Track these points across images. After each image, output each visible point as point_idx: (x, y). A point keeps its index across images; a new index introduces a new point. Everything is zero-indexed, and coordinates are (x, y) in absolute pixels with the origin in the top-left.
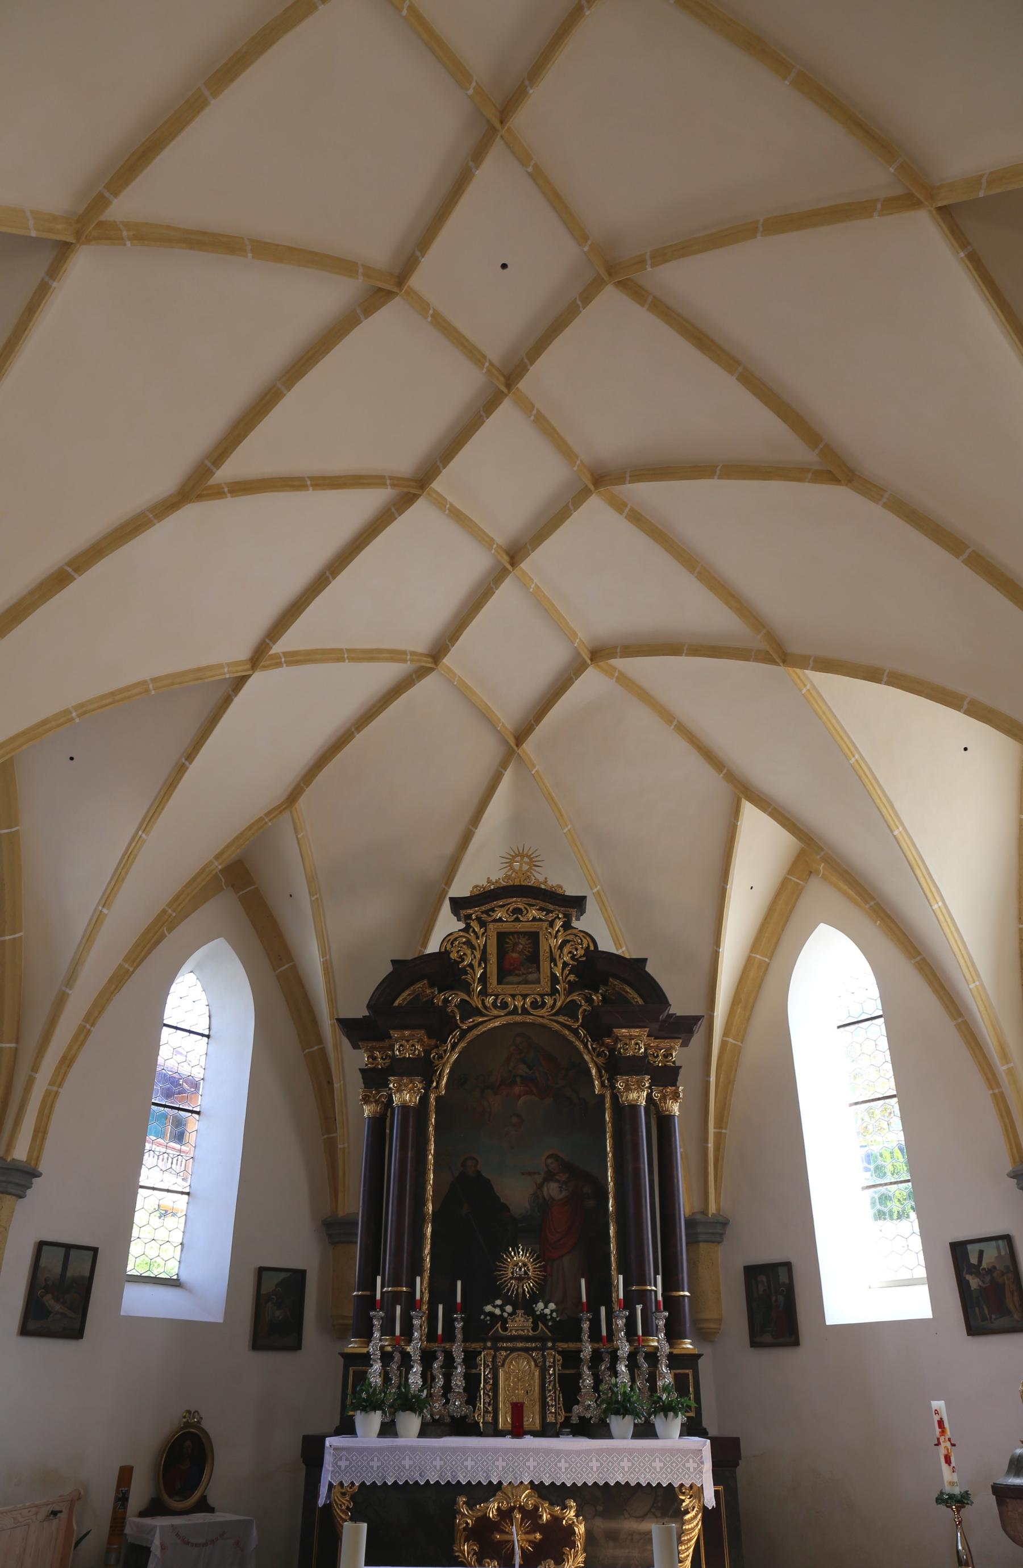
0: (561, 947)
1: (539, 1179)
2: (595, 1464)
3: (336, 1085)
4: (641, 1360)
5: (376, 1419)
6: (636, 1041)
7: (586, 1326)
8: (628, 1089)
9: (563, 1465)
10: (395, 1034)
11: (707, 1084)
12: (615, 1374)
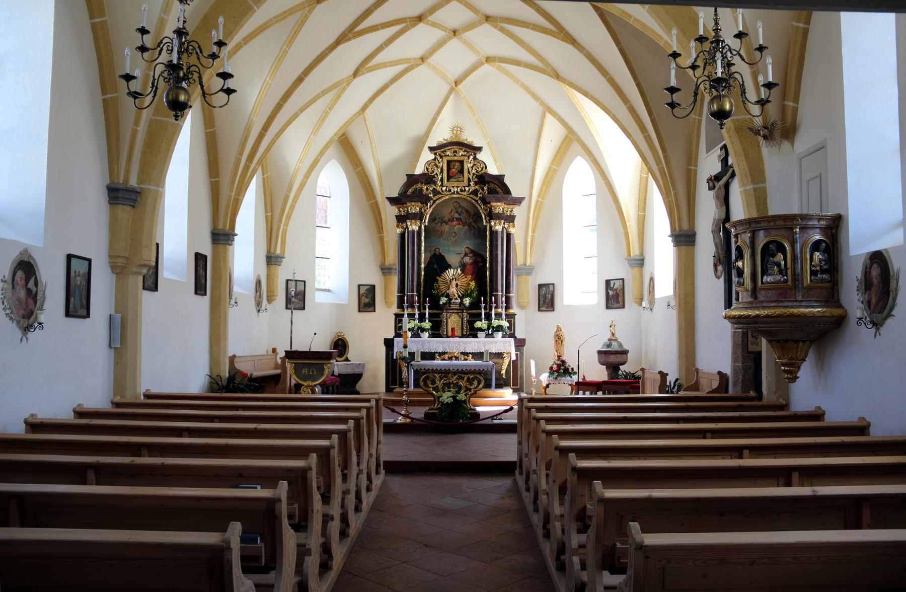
3: (383, 217)
6: (499, 207)
10: (408, 204)
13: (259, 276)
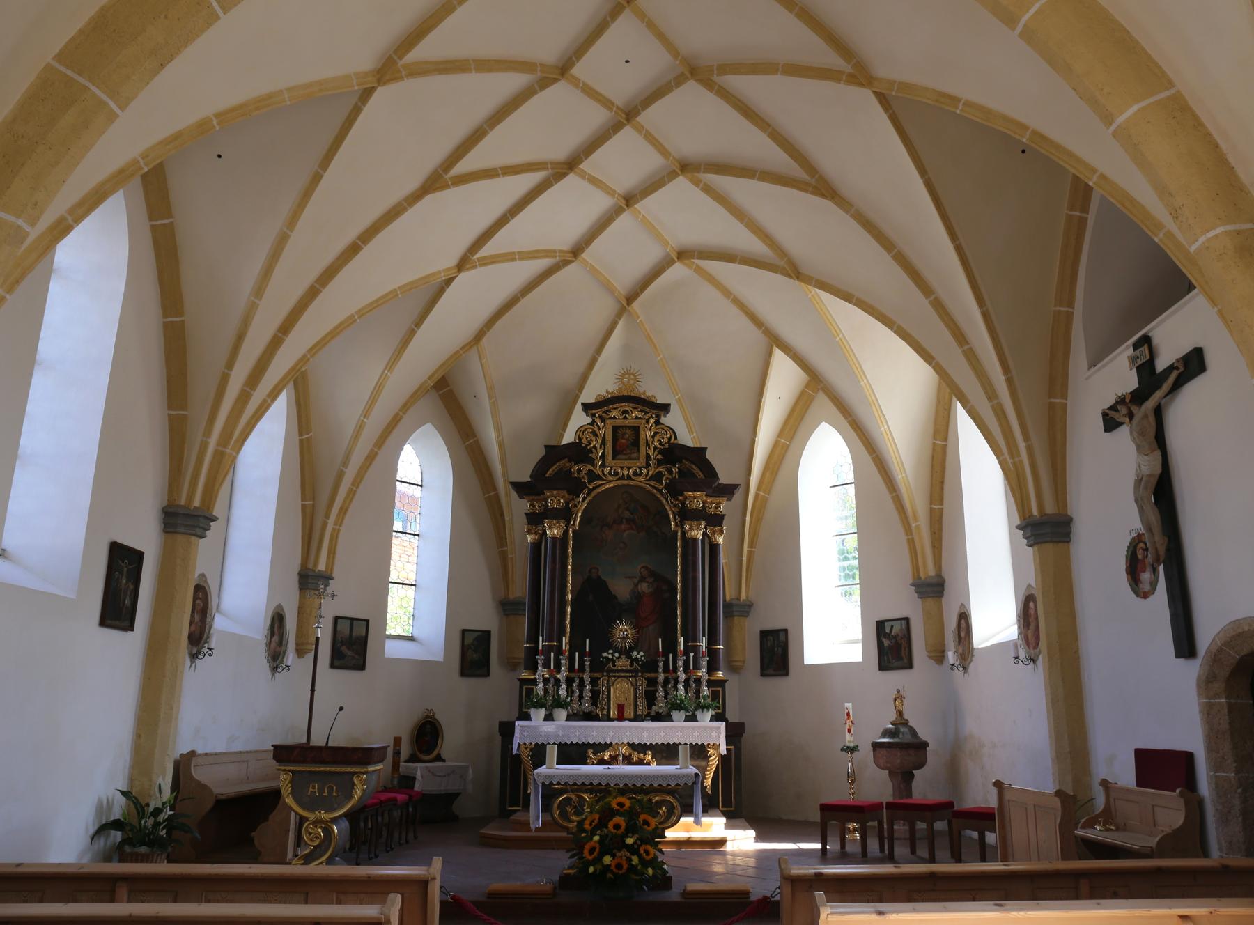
0: (653, 437)
1: (636, 581)
2: (662, 734)
3: (507, 518)
4: (692, 682)
5: (542, 712)
6: (698, 500)
7: (661, 664)
8: (691, 529)
9: (645, 734)
11: (744, 521)
12: (676, 689)
13: (280, 606)
